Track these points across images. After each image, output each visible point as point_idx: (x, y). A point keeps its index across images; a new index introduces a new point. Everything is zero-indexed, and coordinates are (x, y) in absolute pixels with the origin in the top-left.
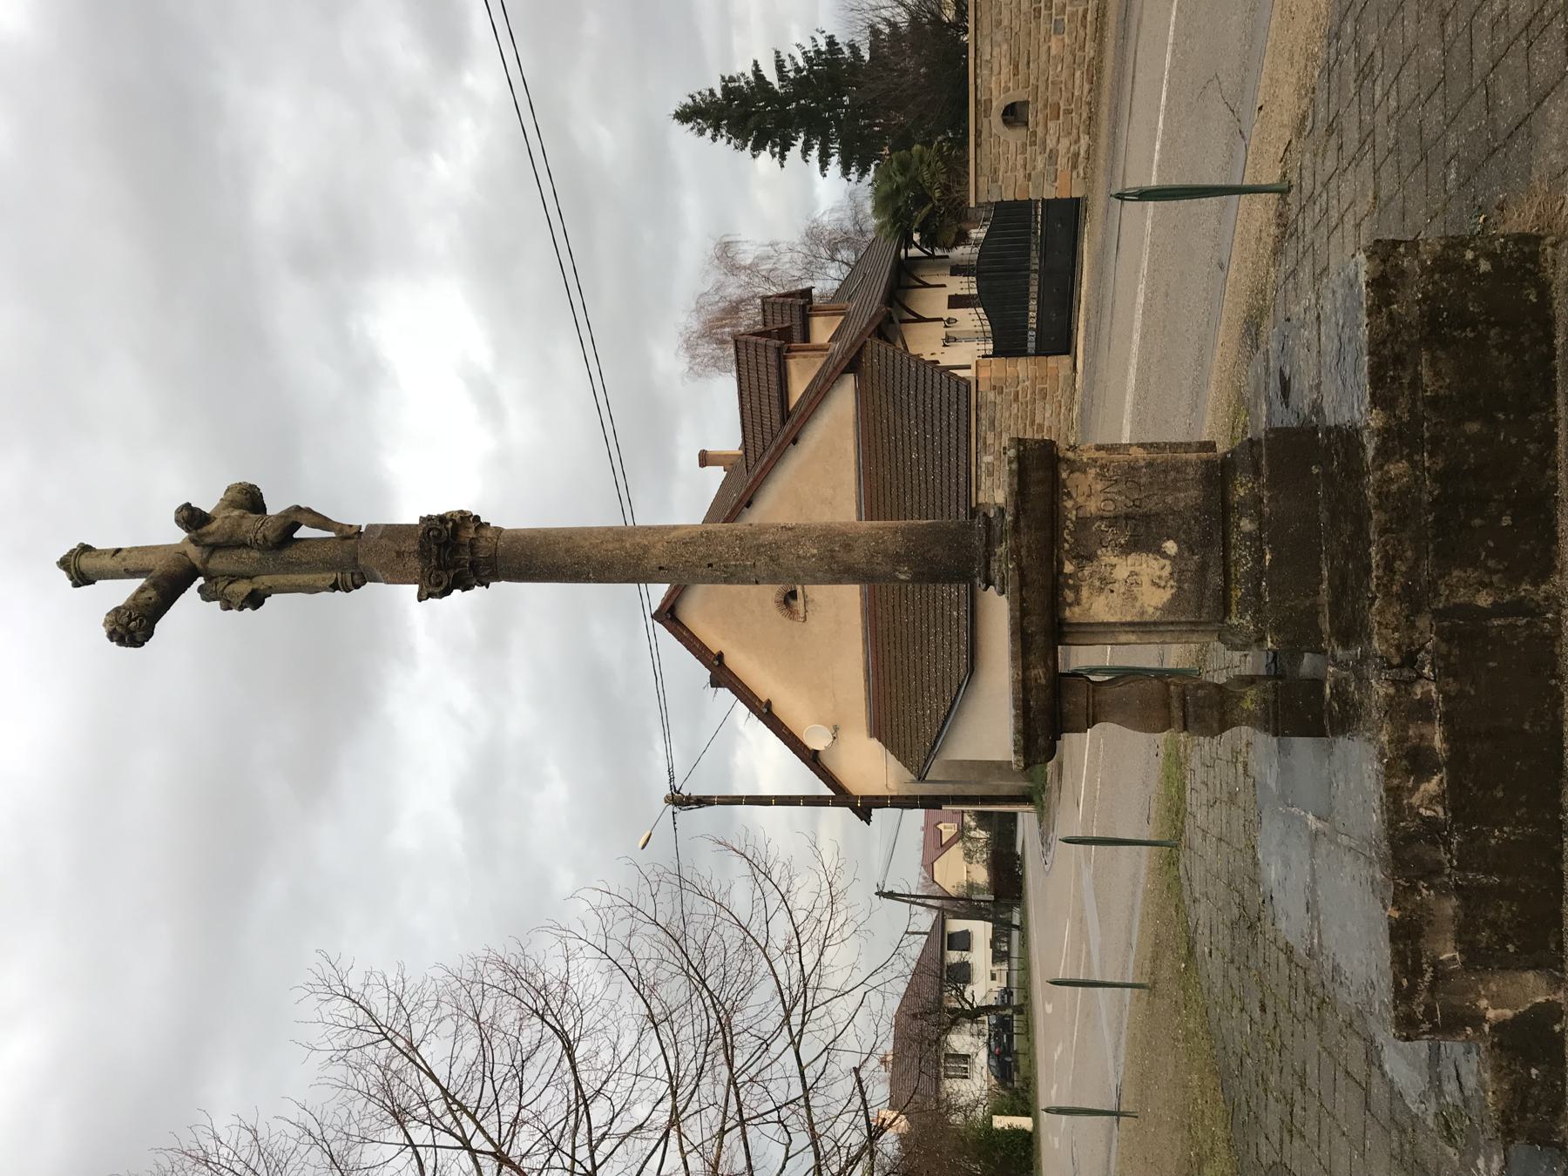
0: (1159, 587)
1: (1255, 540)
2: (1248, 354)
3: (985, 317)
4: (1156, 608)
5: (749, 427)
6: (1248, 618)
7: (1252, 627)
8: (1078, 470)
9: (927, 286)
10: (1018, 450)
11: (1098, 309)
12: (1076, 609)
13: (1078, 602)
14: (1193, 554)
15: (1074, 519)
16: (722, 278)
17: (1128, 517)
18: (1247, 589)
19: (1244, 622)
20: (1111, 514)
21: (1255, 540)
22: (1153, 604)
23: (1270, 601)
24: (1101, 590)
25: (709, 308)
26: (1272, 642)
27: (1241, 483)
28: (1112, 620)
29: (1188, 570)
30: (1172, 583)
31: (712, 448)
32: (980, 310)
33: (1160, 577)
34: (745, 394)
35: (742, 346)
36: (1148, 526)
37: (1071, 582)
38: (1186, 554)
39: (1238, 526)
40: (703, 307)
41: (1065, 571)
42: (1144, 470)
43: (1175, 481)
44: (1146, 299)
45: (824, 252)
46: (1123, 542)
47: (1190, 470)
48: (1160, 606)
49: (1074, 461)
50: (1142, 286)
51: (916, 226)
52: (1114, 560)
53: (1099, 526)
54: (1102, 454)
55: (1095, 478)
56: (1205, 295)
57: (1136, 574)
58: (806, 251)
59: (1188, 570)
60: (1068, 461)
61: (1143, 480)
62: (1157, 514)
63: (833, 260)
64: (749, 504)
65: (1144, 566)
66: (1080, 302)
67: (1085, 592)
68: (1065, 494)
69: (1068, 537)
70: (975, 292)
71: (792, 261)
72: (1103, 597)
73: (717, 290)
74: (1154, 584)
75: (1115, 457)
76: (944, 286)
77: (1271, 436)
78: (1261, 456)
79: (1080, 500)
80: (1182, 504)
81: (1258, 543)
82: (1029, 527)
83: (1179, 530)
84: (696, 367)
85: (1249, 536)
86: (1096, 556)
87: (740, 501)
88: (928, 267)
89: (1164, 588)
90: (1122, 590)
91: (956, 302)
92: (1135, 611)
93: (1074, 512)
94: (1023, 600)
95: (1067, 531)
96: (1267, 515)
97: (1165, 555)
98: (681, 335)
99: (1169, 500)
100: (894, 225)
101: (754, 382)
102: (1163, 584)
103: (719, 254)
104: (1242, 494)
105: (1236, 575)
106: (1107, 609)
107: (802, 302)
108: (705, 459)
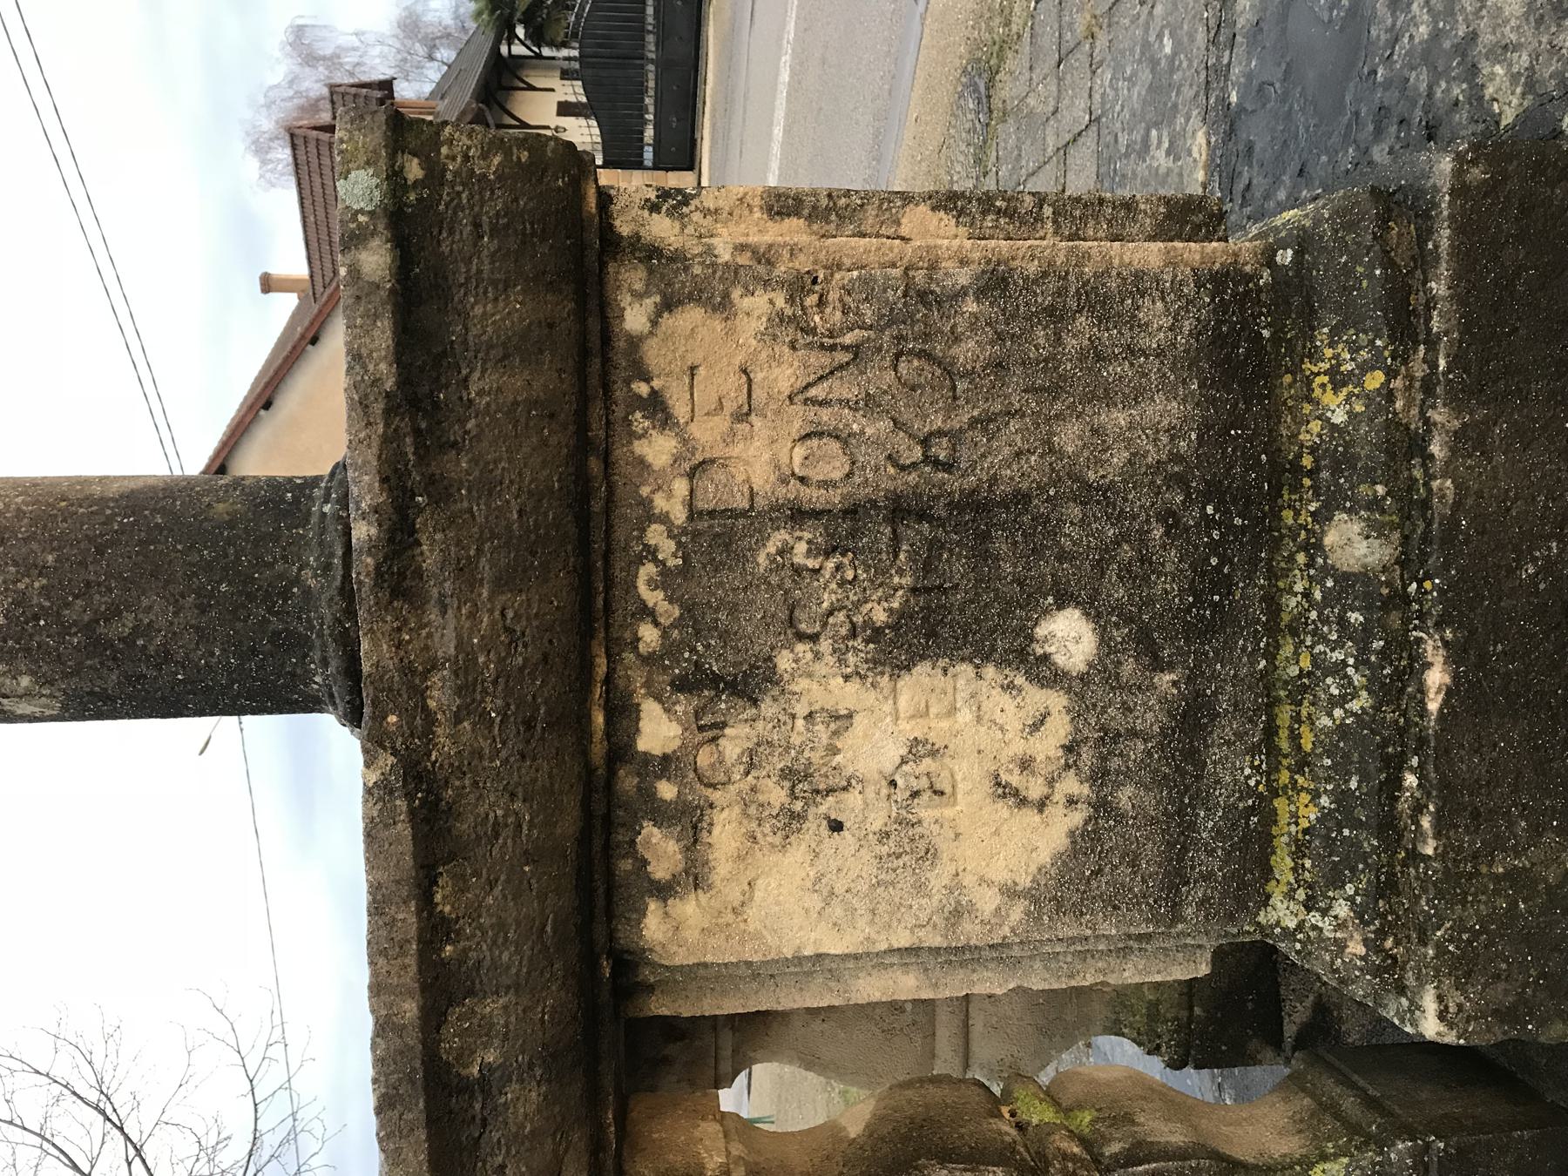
0: (1023, 802)
1: (1387, 604)
2: (968, 126)
3: (582, 91)
4: (1010, 892)
5: (314, 245)
6: (1342, 909)
7: (1356, 948)
8: (697, 295)
9: (534, 89)
10: (395, 178)
11: (729, 58)
12: (690, 908)
13: (695, 876)
14: (1158, 665)
15: (679, 515)
16: (297, 69)
17: (900, 510)
18: (1341, 797)
19: (1326, 925)
20: (835, 498)
21: (1387, 604)
22: (1000, 874)
23: (1441, 856)
24: (793, 820)
25: (282, 104)
26: (1442, 1016)
27: (1333, 372)
28: (835, 945)
29: (1133, 733)
30: (1071, 785)
31: (278, 270)
32: (594, 123)
33: (1026, 764)
34: (307, 203)
35: (300, 142)
36: (982, 554)
37: (667, 790)
38: (1128, 667)
39: (1314, 547)
40: (274, 102)
41: (642, 745)
42: (971, 306)
43: (1096, 355)
44: (793, 74)
45: (421, 50)
46: (880, 617)
47: (1154, 312)
48: (1025, 882)
49: (679, 258)
50: (786, 59)
51: (518, 15)
52: (845, 695)
53: (785, 551)
54: (793, 230)
55: (769, 336)
56: (885, 48)
57: (933, 753)
58: (398, 45)
59: (1133, 733)
60: (651, 254)
61: (967, 352)
62: (1021, 499)
63: (431, 58)
64: (314, 341)
65: (965, 716)
66: (704, 103)
67: (724, 834)
68: (638, 402)
69: (654, 598)
70: (584, 100)
71: (383, 56)
72: (798, 852)
73: (291, 82)
74: (1004, 791)
75: (847, 245)
76: (553, 90)
77: (1477, 174)
78: (1424, 261)
79: (707, 433)
80: (1119, 458)
81: (1395, 620)
82: (465, 572)
83: (1100, 566)
84: (268, 175)
85: (1350, 584)
86: (771, 677)
87: (303, 337)
88: (535, 67)
89: (1041, 805)
90: (877, 822)
91: (565, 109)
92: (925, 907)
93: (681, 487)
94: (435, 929)
95: (647, 570)
96: (1440, 509)
97: (1044, 671)
98: (248, 134)
99: (1069, 437)
100: (492, 12)
101: (318, 189)
102: (1035, 789)
103: (291, 39)
104: (1339, 418)
105: (1295, 737)
106: (815, 902)
107: (378, 94)
108: (268, 284)
